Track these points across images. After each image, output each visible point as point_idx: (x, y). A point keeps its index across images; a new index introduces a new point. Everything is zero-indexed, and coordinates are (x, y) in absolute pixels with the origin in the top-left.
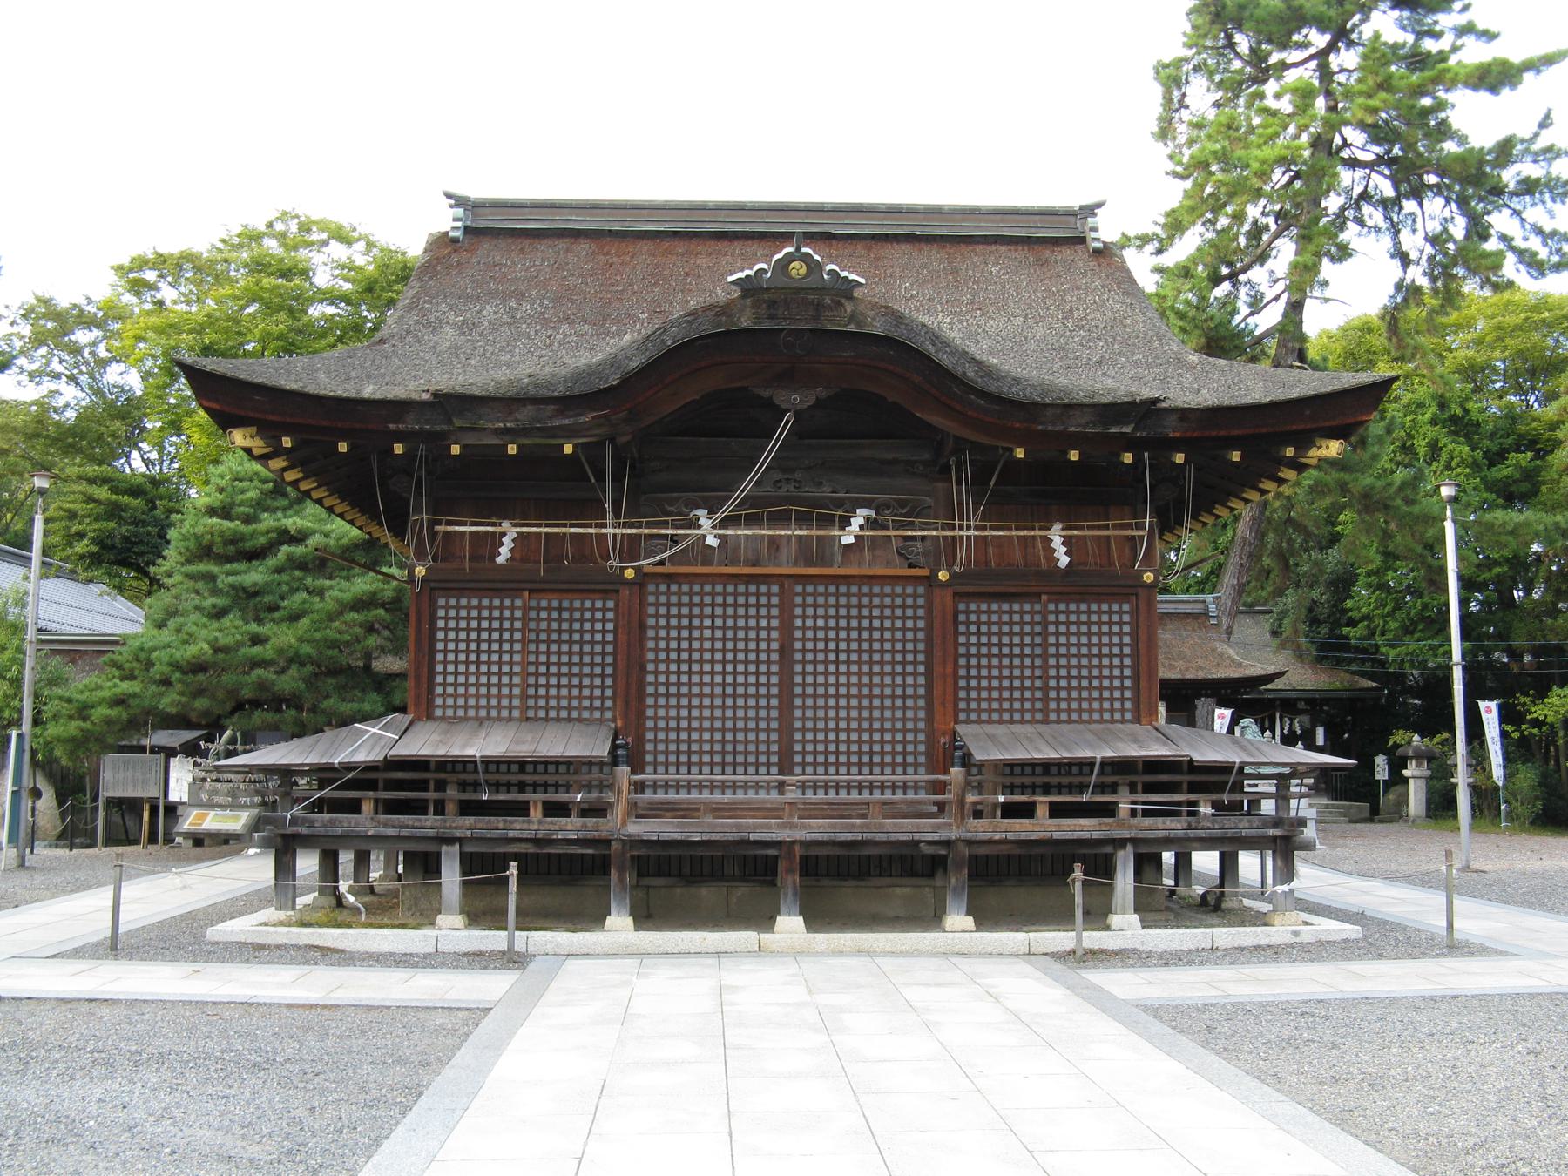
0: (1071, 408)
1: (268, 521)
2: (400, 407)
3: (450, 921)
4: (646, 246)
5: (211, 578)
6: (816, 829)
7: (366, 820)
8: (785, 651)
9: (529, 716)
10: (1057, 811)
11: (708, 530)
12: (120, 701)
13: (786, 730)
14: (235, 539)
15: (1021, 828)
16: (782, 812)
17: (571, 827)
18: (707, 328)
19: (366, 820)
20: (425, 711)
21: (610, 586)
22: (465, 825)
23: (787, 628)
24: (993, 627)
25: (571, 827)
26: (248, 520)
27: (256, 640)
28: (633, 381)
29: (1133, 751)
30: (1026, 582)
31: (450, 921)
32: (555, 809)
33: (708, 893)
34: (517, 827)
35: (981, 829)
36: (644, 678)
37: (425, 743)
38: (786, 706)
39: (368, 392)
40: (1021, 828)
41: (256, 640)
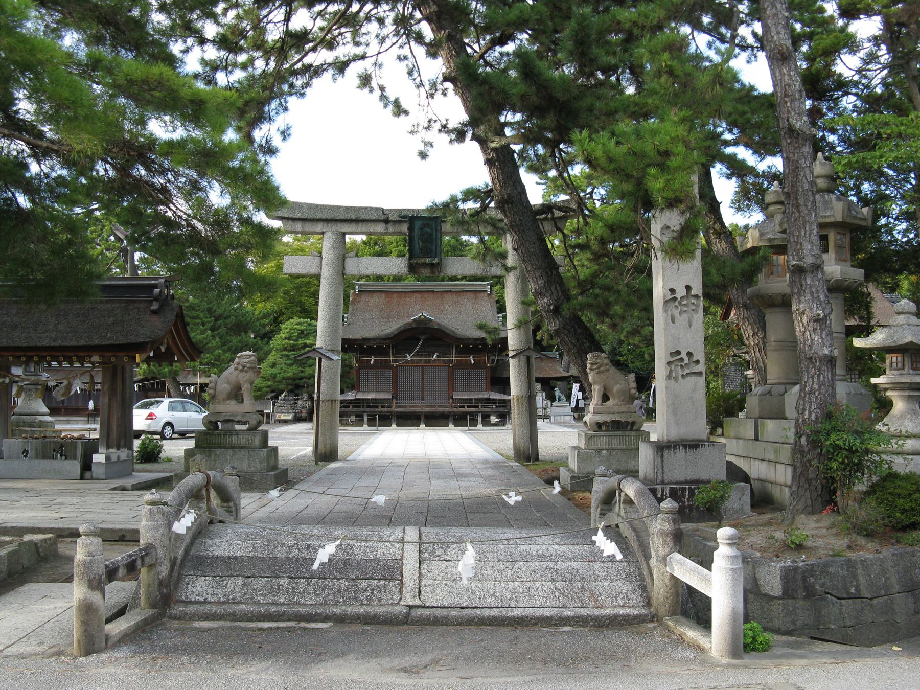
0: (469, 339)
1: (301, 341)
2: (356, 340)
3: (365, 426)
4: (396, 295)
5: (287, 356)
6: (427, 410)
7: (351, 409)
8: (423, 379)
9: (377, 391)
10: (468, 407)
11: (409, 358)
12: (268, 387)
13: (423, 393)
14: (294, 345)
15: (462, 410)
16: (421, 407)
17: (386, 410)
18: (407, 327)
19: (351, 409)
20: (359, 390)
21: (391, 367)
22: (368, 410)
23: (423, 375)
24: (460, 374)
25: (386, 410)
26: (295, 341)
27: (302, 372)
28: (395, 336)
29: (481, 397)
30: (466, 366)
31: (365, 426)
32: (382, 407)
33: (409, 422)
34: (376, 410)
35: (455, 410)
36: (410, 523)
37: (360, 396)
38: (423, 388)
39: (351, 337)
40: (462, 410)
41: (302, 372)
